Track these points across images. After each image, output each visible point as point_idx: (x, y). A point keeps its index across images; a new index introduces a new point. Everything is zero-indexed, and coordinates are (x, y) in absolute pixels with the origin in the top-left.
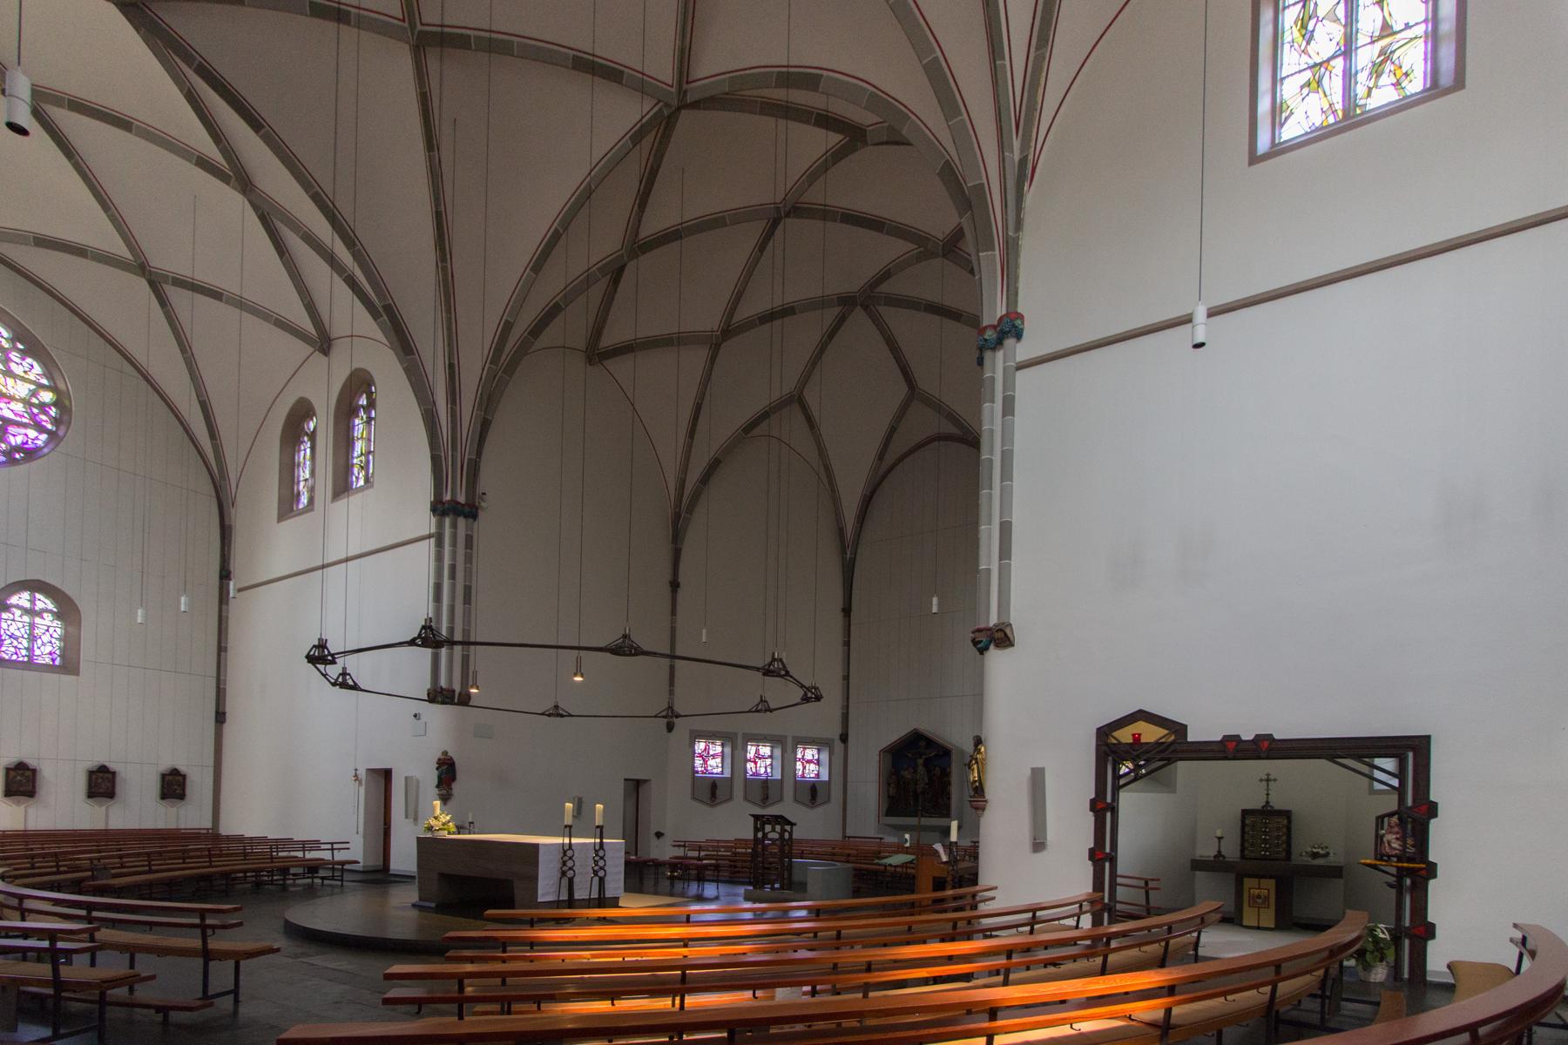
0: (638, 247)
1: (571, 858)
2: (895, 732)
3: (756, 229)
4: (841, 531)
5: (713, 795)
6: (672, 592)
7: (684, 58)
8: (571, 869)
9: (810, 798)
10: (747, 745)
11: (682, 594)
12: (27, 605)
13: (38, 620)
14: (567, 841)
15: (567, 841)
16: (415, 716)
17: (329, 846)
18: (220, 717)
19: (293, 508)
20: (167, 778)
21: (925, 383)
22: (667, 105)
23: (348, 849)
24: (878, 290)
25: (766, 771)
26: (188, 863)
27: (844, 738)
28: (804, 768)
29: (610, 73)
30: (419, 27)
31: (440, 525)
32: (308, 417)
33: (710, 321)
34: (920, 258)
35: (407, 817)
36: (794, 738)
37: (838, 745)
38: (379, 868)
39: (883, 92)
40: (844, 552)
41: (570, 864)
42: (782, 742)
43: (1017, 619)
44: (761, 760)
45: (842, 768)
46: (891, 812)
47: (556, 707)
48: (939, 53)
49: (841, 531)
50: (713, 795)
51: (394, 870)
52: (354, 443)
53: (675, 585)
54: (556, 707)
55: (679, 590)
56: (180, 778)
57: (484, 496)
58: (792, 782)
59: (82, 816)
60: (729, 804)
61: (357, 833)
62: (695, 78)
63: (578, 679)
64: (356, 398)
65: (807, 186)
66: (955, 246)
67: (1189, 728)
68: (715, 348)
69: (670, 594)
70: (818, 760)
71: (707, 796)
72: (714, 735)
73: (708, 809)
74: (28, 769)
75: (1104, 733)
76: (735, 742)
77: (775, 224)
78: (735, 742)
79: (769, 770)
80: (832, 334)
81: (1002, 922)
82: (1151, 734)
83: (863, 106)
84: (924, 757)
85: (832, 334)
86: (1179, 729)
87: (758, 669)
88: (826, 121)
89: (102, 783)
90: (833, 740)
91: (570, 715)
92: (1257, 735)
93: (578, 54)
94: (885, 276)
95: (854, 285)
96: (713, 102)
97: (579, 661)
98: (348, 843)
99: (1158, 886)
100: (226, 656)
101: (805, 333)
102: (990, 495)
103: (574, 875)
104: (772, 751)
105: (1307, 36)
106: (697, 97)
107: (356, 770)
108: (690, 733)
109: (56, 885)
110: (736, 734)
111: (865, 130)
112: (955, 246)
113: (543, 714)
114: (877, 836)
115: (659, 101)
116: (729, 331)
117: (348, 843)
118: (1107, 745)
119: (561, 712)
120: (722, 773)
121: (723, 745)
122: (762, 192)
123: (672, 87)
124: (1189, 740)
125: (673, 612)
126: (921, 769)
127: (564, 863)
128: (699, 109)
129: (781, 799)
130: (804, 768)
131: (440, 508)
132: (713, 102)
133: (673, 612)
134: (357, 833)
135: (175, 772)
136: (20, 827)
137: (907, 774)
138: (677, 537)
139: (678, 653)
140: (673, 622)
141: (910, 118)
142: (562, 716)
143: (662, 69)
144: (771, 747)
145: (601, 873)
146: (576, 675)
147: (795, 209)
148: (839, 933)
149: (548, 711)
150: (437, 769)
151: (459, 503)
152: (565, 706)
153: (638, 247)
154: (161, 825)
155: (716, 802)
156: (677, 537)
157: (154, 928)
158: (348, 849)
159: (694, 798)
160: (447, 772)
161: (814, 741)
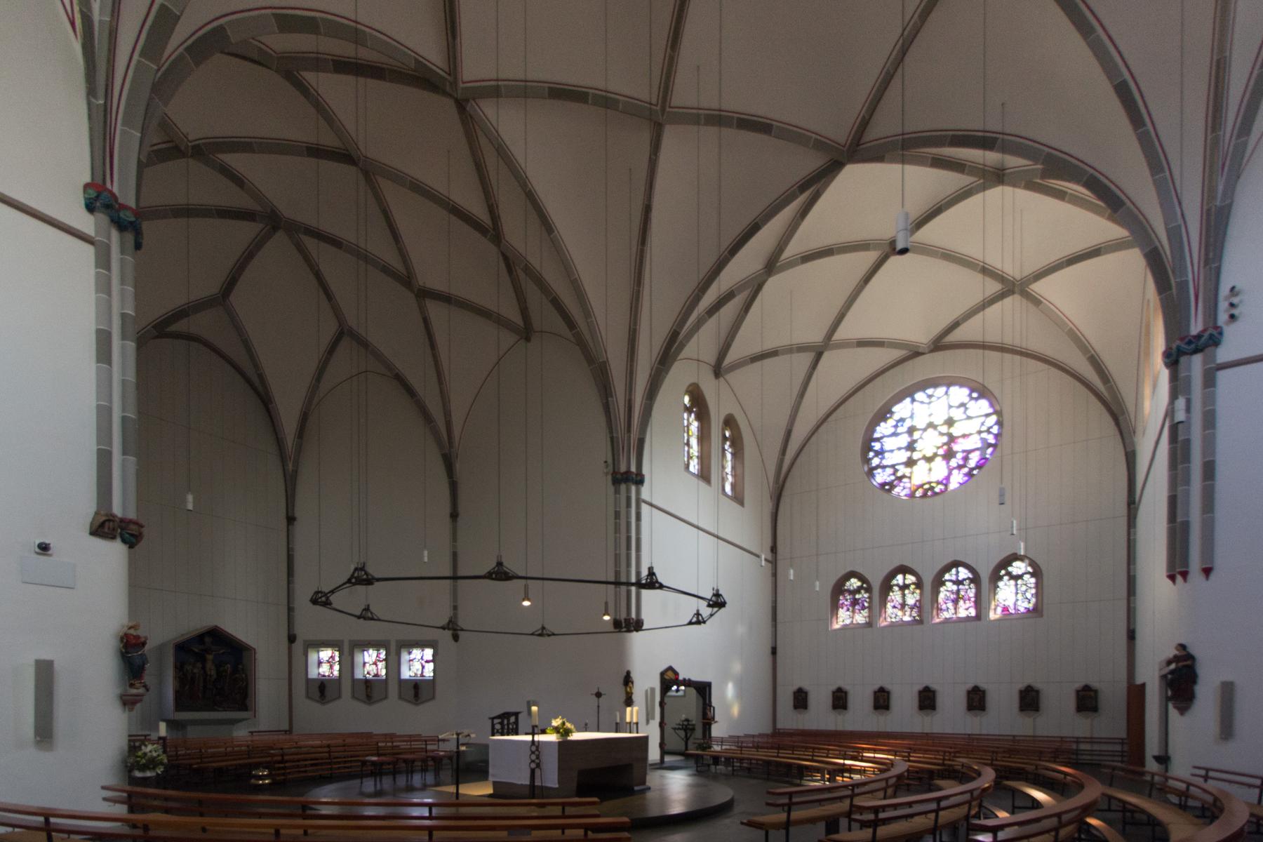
1: (533, 753)
5: (416, 695)
7: (494, 91)
11: (299, 527)
12: (954, 578)
13: (961, 587)
14: (537, 738)
15: (537, 738)
16: (44, 548)
18: (774, 651)
20: (836, 694)
26: (796, 754)
28: (423, 667)
30: (668, 109)
38: (656, 762)
42: (339, 647)
44: (371, 663)
50: (416, 695)
51: (652, 761)
53: (291, 520)
54: (543, 628)
56: (886, 694)
59: (1078, 727)
60: (385, 702)
63: (526, 603)
65: (141, 157)
71: (317, 694)
74: (980, 691)
76: (349, 650)
78: (349, 650)
81: (74, 826)
87: (378, 580)
89: (927, 700)
93: (552, 85)
95: (287, 211)
97: (526, 587)
100: (1135, 599)
102: (124, 373)
109: (132, 744)
110: (342, 642)
113: (532, 634)
114: (140, 733)
127: (538, 757)
129: (339, 697)
130: (423, 667)
135: (840, 690)
136: (1030, 733)
139: (460, 573)
147: (370, 172)
148: (277, 833)
149: (536, 631)
152: (550, 627)
154: (917, 729)
157: (822, 803)
161: (369, 644)
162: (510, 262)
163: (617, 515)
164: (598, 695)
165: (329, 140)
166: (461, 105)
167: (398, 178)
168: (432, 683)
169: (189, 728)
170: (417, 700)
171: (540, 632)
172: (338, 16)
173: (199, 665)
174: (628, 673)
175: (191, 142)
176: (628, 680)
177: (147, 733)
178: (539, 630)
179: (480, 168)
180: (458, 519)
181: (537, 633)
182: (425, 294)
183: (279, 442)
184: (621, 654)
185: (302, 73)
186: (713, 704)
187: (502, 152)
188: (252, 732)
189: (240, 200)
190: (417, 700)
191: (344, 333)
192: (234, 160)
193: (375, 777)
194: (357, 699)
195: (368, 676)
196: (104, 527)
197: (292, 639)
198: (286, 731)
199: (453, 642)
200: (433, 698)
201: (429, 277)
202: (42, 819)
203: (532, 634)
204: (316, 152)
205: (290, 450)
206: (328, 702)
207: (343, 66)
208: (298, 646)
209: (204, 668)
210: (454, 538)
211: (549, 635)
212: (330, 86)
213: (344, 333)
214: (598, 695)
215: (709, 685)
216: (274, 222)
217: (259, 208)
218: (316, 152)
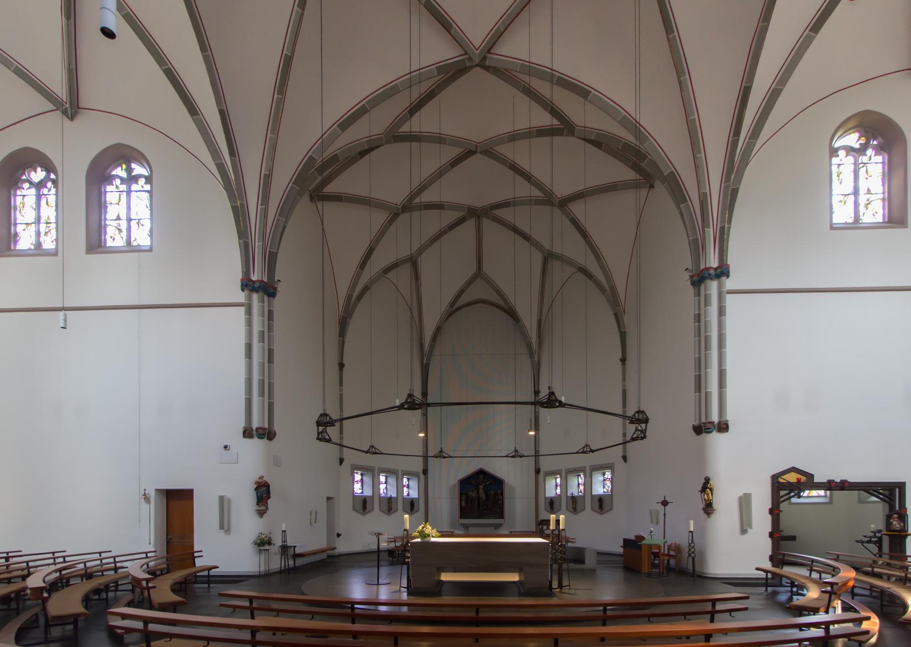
0: (394, 136)
1: (693, 547)
2: (467, 468)
3: (454, 152)
4: (422, 346)
6: (340, 370)
7: (497, 36)
8: (693, 552)
9: (410, 509)
10: (380, 475)
16: (226, 447)
17: (51, 555)
19: (10, 247)
21: (487, 269)
22: (470, 59)
23: (202, 556)
24: (494, 212)
25: (384, 492)
27: (425, 472)
29: (445, 23)
31: (250, 298)
32: (30, 167)
33: (397, 195)
34: (539, 202)
35: (652, 523)
36: (379, 468)
37: (422, 476)
39: (149, 34)
40: (422, 359)
41: (693, 550)
43: (731, 416)
45: (425, 490)
46: (462, 516)
47: (441, 451)
48: (696, 117)
49: (422, 346)
52: (106, 207)
53: (341, 366)
54: (516, 451)
55: (344, 369)
57: (279, 282)
58: (402, 498)
60: (611, 512)
61: (150, 543)
62: (494, 52)
64: (111, 168)
66: (566, 205)
67: (815, 476)
68: (395, 216)
69: (339, 371)
70: (408, 485)
72: (552, 473)
73: (361, 516)
75: (775, 478)
77: (469, 153)
79: (385, 491)
80: (452, 227)
82: (792, 478)
83: (618, 120)
84: (483, 484)
85: (452, 227)
86: (810, 476)
88: (554, 112)
90: (419, 473)
91: (382, 453)
92: (841, 480)
94: (505, 204)
95: (479, 203)
96: (503, 73)
98: (201, 551)
99: (201, 555)
101: (434, 222)
103: (695, 556)
104: (386, 479)
105: (840, 181)
106: (492, 64)
107: (145, 490)
108: (351, 466)
111: (575, 128)
112: (566, 205)
113: (577, 453)
115: (466, 54)
116: (408, 207)
117: (201, 551)
118: (779, 482)
119: (444, 454)
120: (362, 493)
121: (362, 475)
122: (476, 134)
123: (477, 50)
124: (815, 481)
125: (341, 384)
126: (482, 492)
127: (690, 550)
128: (488, 71)
129: (584, 509)
131: (247, 285)
132: (495, 70)
133: (341, 384)
134: (150, 543)
137: (473, 494)
138: (342, 333)
140: (341, 390)
141: (649, 139)
142: (445, 457)
143: (477, 35)
144: (386, 476)
145: (693, 555)
146: (529, 431)
147: (488, 150)
149: (510, 454)
150: (256, 489)
151: (251, 280)
152: (380, 447)
153: (394, 136)
155: (414, 511)
156: (342, 333)
158: (202, 556)
159: (354, 510)
160: (263, 492)
161: (388, 471)
162: (599, 142)
163: (698, 318)
164: (665, 503)
165: (456, 152)
166: (482, 65)
167: (499, 140)
168: (610, 496)
169: (470, 528)
170: (601, 511)
171: (513, 454)
172: (387, 85)
173: (475, 492)
174: (707, 480)
175: (399, 205)
176: (706, 486)
177: (452, 531)
178: (512, 452)
179: (529, 92)
180: (626, 362)
181: (580, 451)
182: (563, 203)
183: (529, 346)
184: (701, 458)
185: (400, 131)
186: (908, 513)
187: (530, 69)
188: (511, 532)
189: (453, 216)
190: (601, 511)
191: (548, 257)
192: (428, 197)
193: (194, 558)
194: (594, 510)
195: (580, 493)
196: (248, 433)
197: (538, 471)
198: (533, 532)
199: (624, 462)
200: (611, 509)
201: (562, 190)
202: (25, 564)
203: (577, 453)
204: (455, 163)
205: (535, 348)
206: (580, 512)
207: (414, 109)
208: (541, 475)
209: (478, 493)
210: (624, 379)
211: (521, 457)
212: (422, 123)
213: (548, 257)
214: (665, 503)
215: (901, 486)
216: (474, 213)
217: (464, 213)
218: (455, 163)
